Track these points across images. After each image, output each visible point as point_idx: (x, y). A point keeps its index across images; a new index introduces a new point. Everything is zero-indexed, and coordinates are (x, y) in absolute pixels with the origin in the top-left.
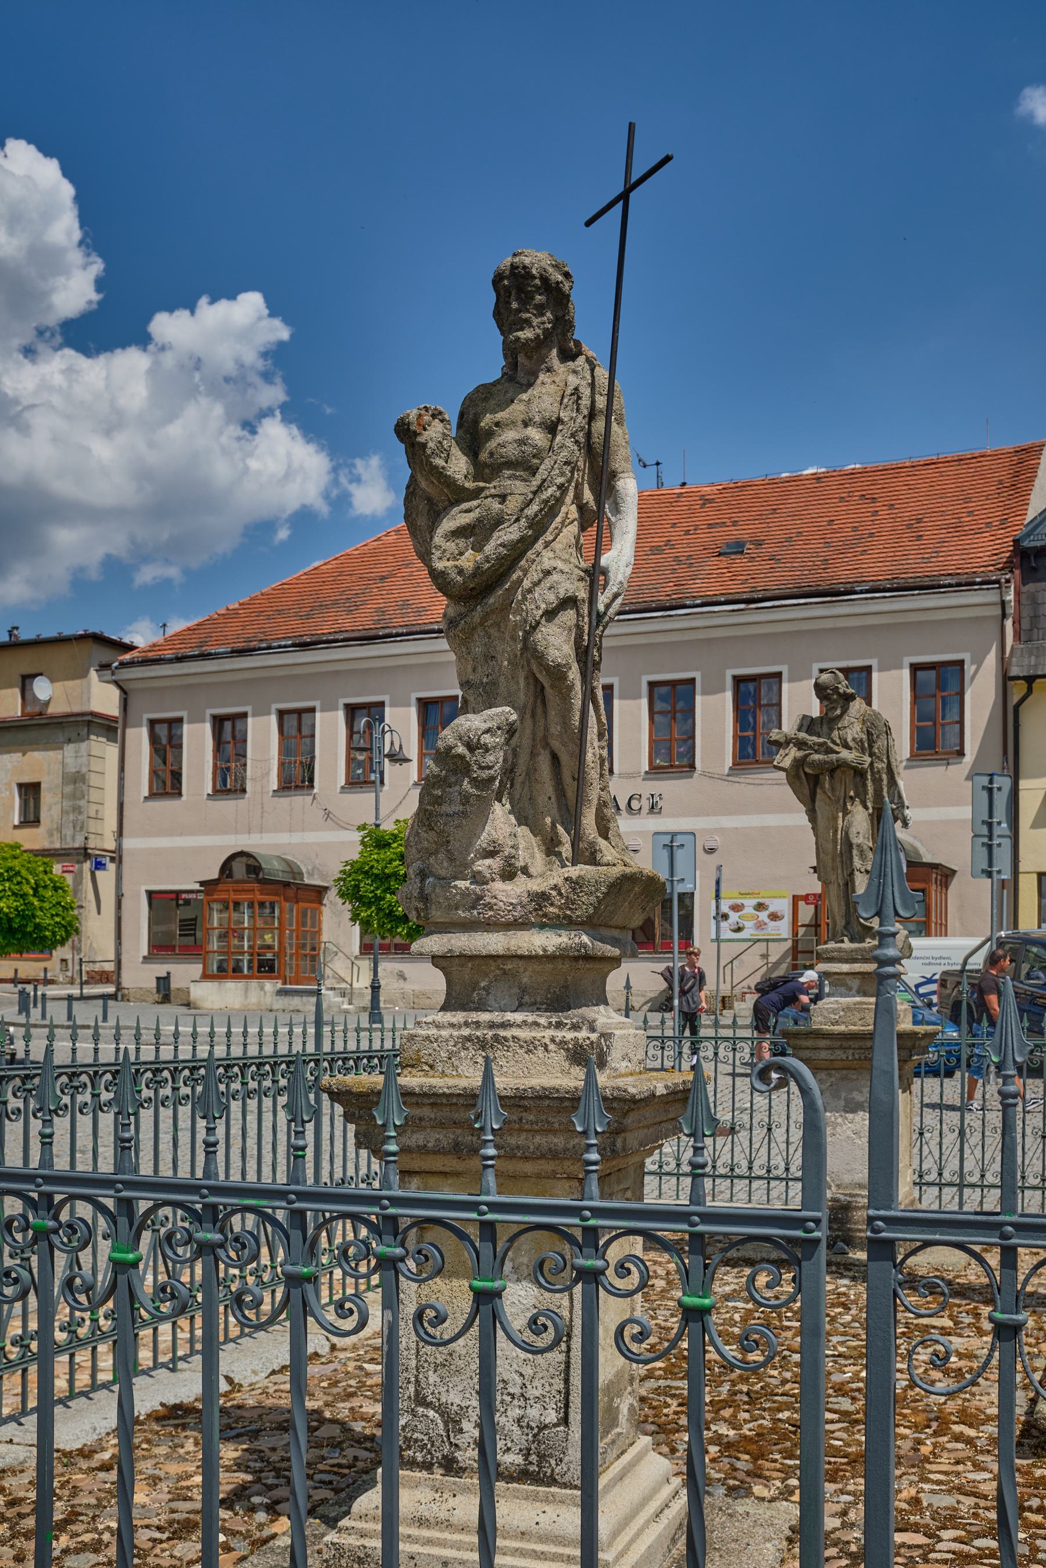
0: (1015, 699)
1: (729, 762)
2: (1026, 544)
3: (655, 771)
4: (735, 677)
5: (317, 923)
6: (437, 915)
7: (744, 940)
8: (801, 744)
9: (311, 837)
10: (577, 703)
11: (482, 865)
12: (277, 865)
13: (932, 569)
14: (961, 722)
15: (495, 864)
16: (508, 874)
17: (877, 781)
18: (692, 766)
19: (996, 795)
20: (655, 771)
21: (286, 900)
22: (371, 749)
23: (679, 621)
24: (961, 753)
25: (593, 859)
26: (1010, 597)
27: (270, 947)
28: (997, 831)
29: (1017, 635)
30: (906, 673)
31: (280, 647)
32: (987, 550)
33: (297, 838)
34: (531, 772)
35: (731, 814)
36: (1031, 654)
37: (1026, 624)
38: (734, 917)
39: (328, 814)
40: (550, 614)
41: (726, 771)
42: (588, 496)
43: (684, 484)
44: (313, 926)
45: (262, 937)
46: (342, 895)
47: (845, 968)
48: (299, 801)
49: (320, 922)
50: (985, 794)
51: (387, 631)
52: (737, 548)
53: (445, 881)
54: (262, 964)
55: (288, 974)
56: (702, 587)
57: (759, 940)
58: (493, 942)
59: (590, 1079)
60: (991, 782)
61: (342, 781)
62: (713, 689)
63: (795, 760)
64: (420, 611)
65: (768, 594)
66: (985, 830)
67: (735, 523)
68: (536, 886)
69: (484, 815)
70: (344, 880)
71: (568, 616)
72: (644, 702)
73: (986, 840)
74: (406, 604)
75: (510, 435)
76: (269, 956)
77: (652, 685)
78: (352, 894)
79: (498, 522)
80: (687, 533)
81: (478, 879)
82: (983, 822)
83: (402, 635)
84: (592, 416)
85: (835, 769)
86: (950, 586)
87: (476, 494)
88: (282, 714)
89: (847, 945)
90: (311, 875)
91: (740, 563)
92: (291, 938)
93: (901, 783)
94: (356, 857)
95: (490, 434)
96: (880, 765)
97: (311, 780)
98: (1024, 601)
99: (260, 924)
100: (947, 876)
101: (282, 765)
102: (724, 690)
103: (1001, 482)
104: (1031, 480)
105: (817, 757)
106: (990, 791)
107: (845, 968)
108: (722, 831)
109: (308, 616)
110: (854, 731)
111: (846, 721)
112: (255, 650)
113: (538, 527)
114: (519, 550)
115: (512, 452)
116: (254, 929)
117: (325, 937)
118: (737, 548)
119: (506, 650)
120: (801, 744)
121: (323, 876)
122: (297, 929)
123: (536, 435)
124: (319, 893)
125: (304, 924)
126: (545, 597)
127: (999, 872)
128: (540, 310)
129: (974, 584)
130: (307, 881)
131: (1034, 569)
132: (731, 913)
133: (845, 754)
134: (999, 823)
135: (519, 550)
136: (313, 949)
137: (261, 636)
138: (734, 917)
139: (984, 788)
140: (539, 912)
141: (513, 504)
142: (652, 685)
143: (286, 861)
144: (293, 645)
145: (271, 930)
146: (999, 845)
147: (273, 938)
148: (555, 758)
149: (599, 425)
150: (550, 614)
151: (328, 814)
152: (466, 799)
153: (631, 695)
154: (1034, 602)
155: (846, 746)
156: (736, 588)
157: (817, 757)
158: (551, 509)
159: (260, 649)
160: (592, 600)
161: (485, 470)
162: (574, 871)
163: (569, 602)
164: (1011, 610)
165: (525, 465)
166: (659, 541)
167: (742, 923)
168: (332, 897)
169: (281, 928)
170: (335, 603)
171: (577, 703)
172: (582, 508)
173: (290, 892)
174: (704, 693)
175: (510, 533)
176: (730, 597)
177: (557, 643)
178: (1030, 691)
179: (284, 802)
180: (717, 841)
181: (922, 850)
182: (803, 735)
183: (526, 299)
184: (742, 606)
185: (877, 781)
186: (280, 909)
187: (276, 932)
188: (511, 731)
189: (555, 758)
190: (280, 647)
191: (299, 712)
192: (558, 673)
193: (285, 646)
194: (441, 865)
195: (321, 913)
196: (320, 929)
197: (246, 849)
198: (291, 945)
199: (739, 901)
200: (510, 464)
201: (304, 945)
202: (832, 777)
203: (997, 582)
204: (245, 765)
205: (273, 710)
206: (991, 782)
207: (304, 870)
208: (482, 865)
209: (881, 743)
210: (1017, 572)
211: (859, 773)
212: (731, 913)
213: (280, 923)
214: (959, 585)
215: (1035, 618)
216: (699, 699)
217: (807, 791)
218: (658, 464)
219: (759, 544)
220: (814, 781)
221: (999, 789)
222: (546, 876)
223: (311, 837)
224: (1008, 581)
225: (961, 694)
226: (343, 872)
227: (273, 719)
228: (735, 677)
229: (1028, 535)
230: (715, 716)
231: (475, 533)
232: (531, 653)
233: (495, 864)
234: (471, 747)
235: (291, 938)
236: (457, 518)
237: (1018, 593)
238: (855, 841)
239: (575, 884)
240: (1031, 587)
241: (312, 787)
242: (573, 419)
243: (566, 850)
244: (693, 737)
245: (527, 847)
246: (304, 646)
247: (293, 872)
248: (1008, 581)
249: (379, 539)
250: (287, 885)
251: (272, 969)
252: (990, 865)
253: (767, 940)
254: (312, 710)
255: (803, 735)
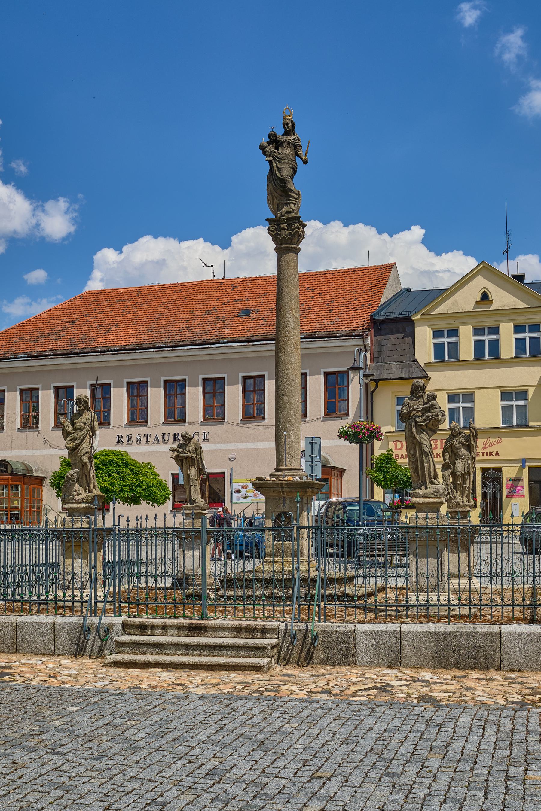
0: (372, 389)
1: (241, 417)
2: (376, 317)
3: (206, 421)
4: (243, 377)
5: (40, 495)
6: (67, 501)
7: (248, 502)
8: (178, 451)
9: (37, 452)
10: (89, 468)
11: (74, 493)
12: (20, 466)
13: (333, 328)
14: (348, 400)
15: (76, 493)
16: (78, 495)
17: (198, 461)
18: (223, 419)
19: (314, 445)
20: (206, 421)
21: (25, 484)
22: (66, 414)
23: (216, 350)
24: (347, 414)
25: (92, 493)
26: (369, 342)
27: (16, 507)
28: (315, 459)
29: (372, 360)
30: (322, 377)
31: (21, 357)
32: (359, 319)
33: (29, 453)
34: (82, 478)
35: (242, 442)
36: (378, 369)
37: (376, 355)
38: (243, 491)
39: (46, 441)
40: (84, 455)
41: (239, 422)
42: (91, 434)
43: (224, 277)
44: (38, 496)
45: (13, 503)
46: (52, 486)
47: (188, 511)
48: (31, 434)
49: (42, 494)
50: (310, 445)
51: (75, 351)
52: (247, 313)
53: (68, 496)
54: (12, 515)
55: (26, 521)
56: (228, 333)
57: (253, 502)
58: (75, 506)
59: (90, 526)
60: (312, 440)
61: (52, 424)
62: (233, 383)
63: (176, 455)
64: (92, 341)
65: (258, 338)
66: (310, 459)
67: (247, 300)
68: (82, 497)
69: (74, 485)
70: (53, 480)
71: (87, 455)
72: (200, 388)
73: (310, 463)
74: (84, 337)
75: (78, 424)
76: (16, 512)
77: (204, 380)
78: (56, 485)
79: (77, 439)
80: (224, 304)
81: (73, 496)
82: (310, 456)
83: (83, 353)
84: (91, 421)
85: (187, 458)
86: (341, 336)
87: (73, 433)
88: (22, 391)
89: (189, 505)
90: (37, 471)
91: (248, 320)
92: (27, 503)
93: (204, 462)
94: (58, 470)
95: (75, 424)
96: (199, 457)
97: (37, 423)
98: (375, 343)
99: (11, 496)
100: (341, 472)
101: (22, 416)
102: (238, 383)
103: (371, 284)
104: (385, 284)
105: (181, 455)
106: (312, 444)
107: (188, 511)
108: (237, 450)
109: (36, 341)
110: (191, 447)
111: (190, 445)
112: (8, 359)
113: (82, 440)
114: (79, 444)
115: (79, 427)
116: (8, 498)
117: (44, 502)
118: (247, 313)
119: (78, 459)
120: (178, 451)
121: (43, 472)
122: (30, 498)
123: (82, 425)
124: (42, 480)
125: (34, 496)
126: (83, 452)
127: (316, 476)
128: (83, 405)
129: (352, 336)
130: (35, 474)
131: (380, 329)
132: (242, 490)
133: (189, 454)
134: (316, 456)
135: (79, 444)
136: (38, 508)
137: (12, 352)
138: (243, 491)
139: (309, 443)
140: (82, 501)
141: (79, 436)
142: (204, 380)
143: (24, 464)
144: (28, 357)
145: (17, 499)
146: (316, 465)
147: (18, 503)
148: (86, 476)
149: (92, 423)
150: (84, 455)
151: (46, 441)
152: (71, 483)
153: (194, 385)
154: (380, 345)
155: (190, 452)
156: (244, 334)
157: (181, 455)
158: (85, 437)
159: (11, 358)
160: (91, 452)
161: (75, 429)
162: (88, 494)
163: (87, 452)
164: (369, 348)
165: (81, 430)
166: (210, 308)
167: (247, 494)
168: (47, 483)
169: (22, 498)
170: (49, 335)
171: (89, 468)
172: (90, 436)
173: (27, 480)
174: (228, 385)
175: (78, 441)
176: (240, 339)
177: (85, 459)
178: (377, 386)
179: (23, 435)
180: (235, 455)
181: (330, 460)
182: (178, 449)
183: (81, 403)
184: (246, 344)
185: (198, 461)
186: (22, 488)
187: (19, 500)
188: (78, 473)
189: (86, 476)
190: (21, 357)
191: (31, 390)
192: (86, 464)
193: (24, 357)
194: (67, 494)
195: (42, 490)
196: (42, 498)
197: (4, 459)
198: (27, 506)
199: (246, 484)
200: (78, 429)
201: (34, 506)
202: (186, 460)
203: (362, 335)
204: (3, 416)
205: (18, 389)
206: (312, 440)
207: (34, 469)
208: (74, 493)
209: (199, 451)
210: (372, 330)
211: (193, 459)
212: (242, 490)
213: (21, 495)
214: (345, 336)
215: (380, 352)
216: (226, 387)
217: (180, 464)
218: (212, 266)
219: (257, 311)
220: (182, 461)
221: (316, 443)
222: (84, 495)
223: (37, 452)
224: (367, 335)
225: (347, 387)
226: (53, 476)
227: (18, 393)
228: (243, 377)
229: (378, 313)
230: (234, 396)
231: (74, 440)
232: (81, 461)
233: (76, 493)
234: (71, 476)
235: (27, 503)
236: (70, 438)
237: (372, 340)
238: (191, 477)
239: (88, 496)
240: (378, 337)
241: (38, 427)
242: (88, 423)
243: (88, 491)
244: (224, 405)
245: (81, 490)
246: (33, 357)
247: (28, 470)
248: (367, 335)
249: (71, 301)
250: (25, 476)
251: (17, 519)
252: (312, 473)
253: (257, 503)
254: (38, 389)
255: (178, 449)
